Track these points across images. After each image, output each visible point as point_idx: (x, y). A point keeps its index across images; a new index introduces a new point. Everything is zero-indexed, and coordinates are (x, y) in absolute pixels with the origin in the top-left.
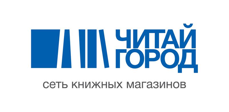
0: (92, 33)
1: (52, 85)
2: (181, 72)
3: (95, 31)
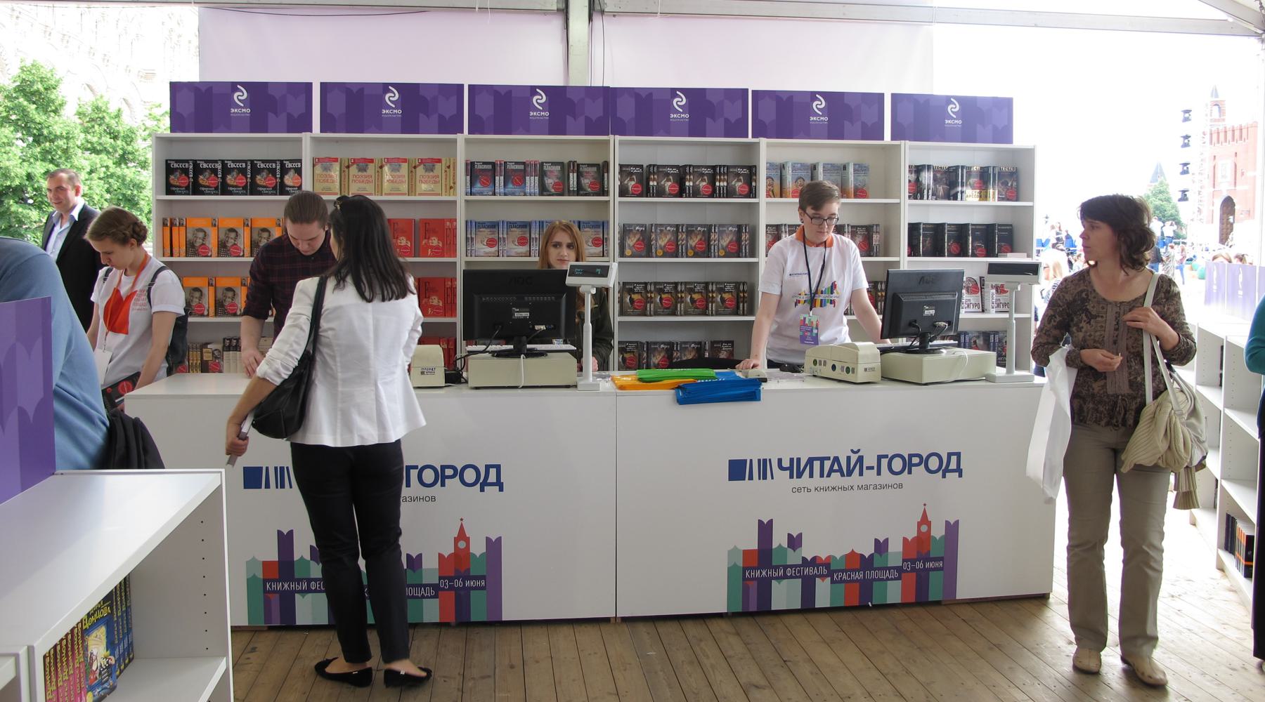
0: (765, 460)
1: (799, 490)
2: (484, 491)
3: (766, 460)
